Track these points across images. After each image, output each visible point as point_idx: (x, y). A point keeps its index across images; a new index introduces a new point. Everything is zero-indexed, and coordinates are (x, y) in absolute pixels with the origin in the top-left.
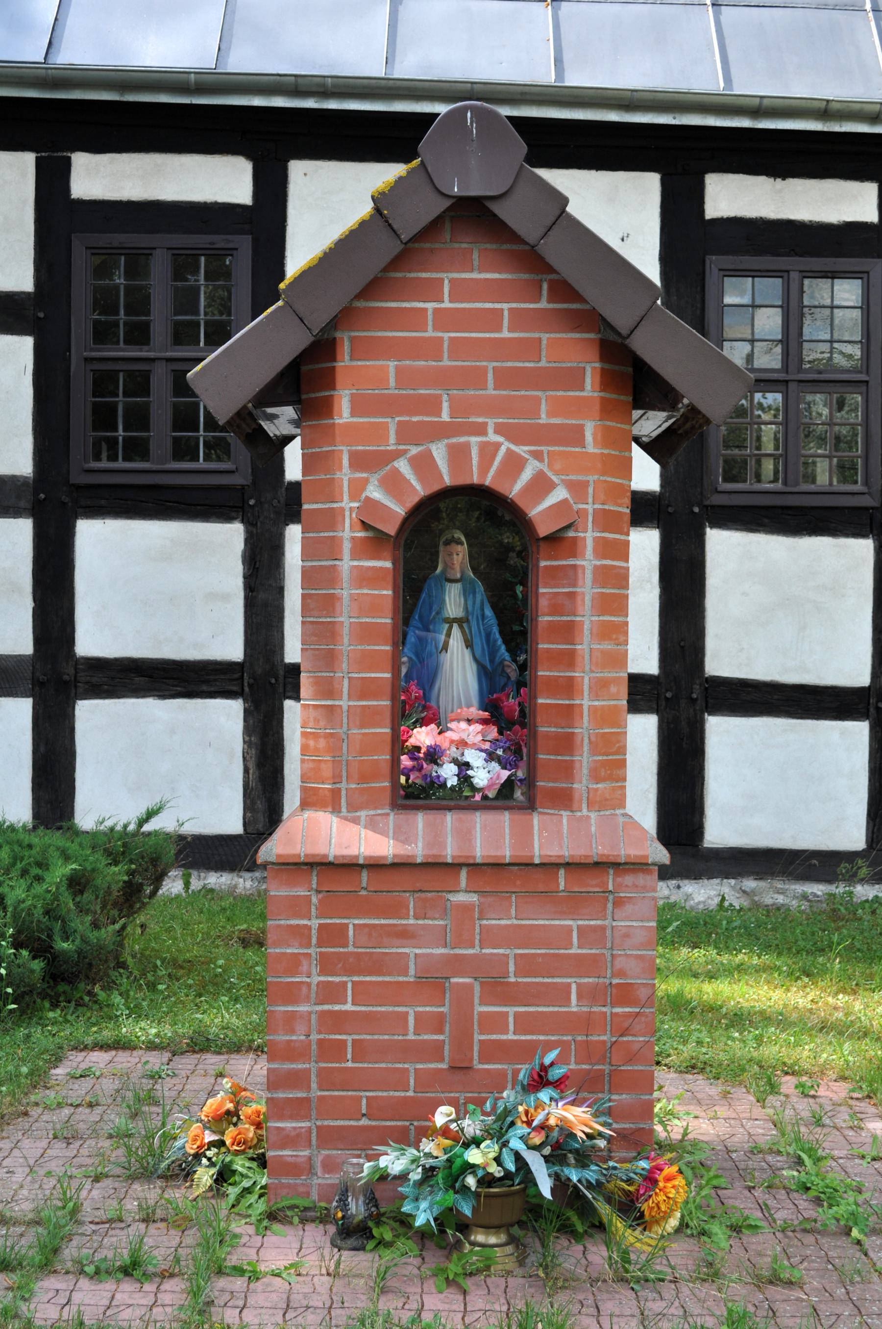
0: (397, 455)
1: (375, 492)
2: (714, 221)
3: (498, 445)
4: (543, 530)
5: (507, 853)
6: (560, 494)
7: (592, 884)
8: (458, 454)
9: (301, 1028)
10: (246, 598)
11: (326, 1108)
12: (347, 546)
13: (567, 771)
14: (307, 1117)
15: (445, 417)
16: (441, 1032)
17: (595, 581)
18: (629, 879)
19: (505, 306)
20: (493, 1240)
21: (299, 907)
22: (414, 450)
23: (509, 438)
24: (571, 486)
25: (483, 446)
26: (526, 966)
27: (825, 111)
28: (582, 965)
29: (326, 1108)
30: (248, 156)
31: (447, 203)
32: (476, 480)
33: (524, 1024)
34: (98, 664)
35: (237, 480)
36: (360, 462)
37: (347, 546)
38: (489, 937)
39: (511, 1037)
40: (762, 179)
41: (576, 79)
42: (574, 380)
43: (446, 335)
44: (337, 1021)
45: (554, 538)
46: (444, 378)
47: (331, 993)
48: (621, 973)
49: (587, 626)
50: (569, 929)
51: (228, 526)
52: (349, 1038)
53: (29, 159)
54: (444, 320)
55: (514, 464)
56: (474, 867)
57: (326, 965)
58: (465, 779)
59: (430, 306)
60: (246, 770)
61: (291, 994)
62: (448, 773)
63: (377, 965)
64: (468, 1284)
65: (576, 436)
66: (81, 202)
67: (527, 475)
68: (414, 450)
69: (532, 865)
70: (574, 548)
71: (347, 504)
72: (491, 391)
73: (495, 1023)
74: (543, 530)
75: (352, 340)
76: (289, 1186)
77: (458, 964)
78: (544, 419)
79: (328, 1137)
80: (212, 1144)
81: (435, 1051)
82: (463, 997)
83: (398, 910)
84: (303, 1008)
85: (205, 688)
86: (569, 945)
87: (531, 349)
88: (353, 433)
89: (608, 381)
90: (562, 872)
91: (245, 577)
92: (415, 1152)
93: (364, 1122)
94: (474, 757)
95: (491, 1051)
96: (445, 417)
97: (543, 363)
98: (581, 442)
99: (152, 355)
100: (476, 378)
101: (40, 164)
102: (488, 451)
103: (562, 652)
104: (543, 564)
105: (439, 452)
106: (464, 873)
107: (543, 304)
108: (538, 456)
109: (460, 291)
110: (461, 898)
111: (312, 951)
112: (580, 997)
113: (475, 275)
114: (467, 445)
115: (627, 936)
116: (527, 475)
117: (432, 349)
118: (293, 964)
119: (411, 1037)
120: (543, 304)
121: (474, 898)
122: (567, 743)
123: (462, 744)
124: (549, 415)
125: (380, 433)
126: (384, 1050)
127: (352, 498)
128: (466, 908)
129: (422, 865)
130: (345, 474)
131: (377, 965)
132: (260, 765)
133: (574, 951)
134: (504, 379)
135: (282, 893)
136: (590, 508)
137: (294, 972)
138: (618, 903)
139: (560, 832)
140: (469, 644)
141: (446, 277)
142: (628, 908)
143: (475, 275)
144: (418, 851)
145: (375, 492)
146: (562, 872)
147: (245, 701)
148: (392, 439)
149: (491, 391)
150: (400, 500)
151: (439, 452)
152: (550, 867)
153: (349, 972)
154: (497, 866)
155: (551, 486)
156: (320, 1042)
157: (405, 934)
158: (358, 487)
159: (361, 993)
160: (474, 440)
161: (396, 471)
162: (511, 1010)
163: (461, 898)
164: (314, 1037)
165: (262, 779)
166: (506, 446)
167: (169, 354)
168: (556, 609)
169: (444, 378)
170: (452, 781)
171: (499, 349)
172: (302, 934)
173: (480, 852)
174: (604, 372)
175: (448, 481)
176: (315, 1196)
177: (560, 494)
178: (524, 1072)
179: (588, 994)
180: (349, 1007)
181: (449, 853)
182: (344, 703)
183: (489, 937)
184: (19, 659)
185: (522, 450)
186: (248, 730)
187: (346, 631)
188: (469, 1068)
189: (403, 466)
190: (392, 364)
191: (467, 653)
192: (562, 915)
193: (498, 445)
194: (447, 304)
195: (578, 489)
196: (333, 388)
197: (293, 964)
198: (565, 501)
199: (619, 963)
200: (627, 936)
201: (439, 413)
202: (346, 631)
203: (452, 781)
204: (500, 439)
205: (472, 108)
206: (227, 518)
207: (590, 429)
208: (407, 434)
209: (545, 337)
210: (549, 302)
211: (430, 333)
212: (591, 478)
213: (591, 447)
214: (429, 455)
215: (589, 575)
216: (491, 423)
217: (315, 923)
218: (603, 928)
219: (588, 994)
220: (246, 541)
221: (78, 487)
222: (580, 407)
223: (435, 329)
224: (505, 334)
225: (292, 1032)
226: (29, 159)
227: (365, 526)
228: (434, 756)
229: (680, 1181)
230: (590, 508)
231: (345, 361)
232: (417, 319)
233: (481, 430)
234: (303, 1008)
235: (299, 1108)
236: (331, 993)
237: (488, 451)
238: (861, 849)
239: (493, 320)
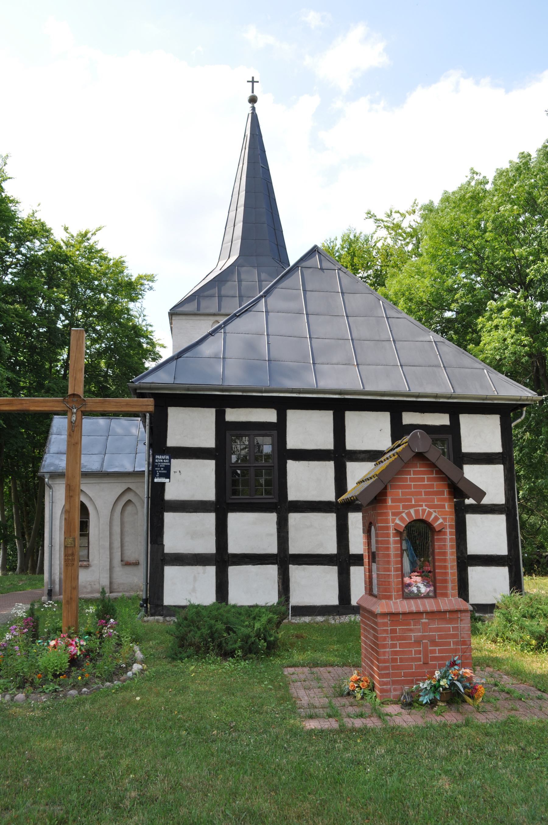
0: (403, 512)
1: (397, 521)
2: (405, 425)
3: (426, 509)
4: (437, 530)
5: (435, 609)
6: (441, 521)
7: (455, 616)
8: (417, 512)
9: (387, 655)
10: (278, 535)
11: (394, 675)
12: (391, 535)
13: (446, 588)
14: (389, 677)
15: (413, 503)
16: (420, 654)
17: (450, 542)
18: (463, 614)
19: (426, 476)
20: (443, 705)
21: (385, 624)
22: (406, 511)
23: (428, 507)
24: (443, 519)
25: (422, 510)
26: (440, 637)
27: (436, 396)
28: (454, 636)
29: (394, 675)
30: (275, 409)
31: (414, 454)
32: (421, 518)
33: (440, 651)
34: (235, 556)
35: (275, 501)
36: (394, 514)
37: (391, 535)
38: (431, 630)
39: (437, 655)
40: (418, 413)
41: (368, 388)
42: (442, 493)
43: (412, 483)
44: (395, 653)
45: (440, 531)
46: (412, 494)
47: (394, 646)
48: (463, 638)
49: (449, 552)
50: (450, 627)
51: (272, 514)
52: (398, 657)
53: (213, 411)
54: (412, 480)
55: (430, 514)
56: (427, 613)
57: (392, 639)
58: (419, 591)
59: (408, 476)
60: (279, 586)
61: (384, 646)
62: (415, 589)
63: (404, 638)
64: (442, 714)
65: (443, 507)
66: (228, 422)
67: (433, 516)
68: (406, 511)
69: (441, 612)
70: (445, 534)
71: (391, 524)
72: (423, 496)
73: (433, 651)
74: (437, 530)
75: (391, 485)
76: (385, 695)
77: (424, 637)
78: (436, 503)
79: (394, 682)
80: (357, 687)
81: (419, 659)
82: (425, 647)
83: (409, 624)
84: (387, 650)
85: (266, 562)
86: (450, 631)
87: (432, 486)
88: (392, 507)
89: (450, 493)
90: (448, 613)
91: (277, 529)
92: (333, 702)
93: (403, 678)
94: (420, 585)
95: (434, 659)
96: (413, 503)
97: (435, 490)
98: (445, 508)
99: (249, 465)
100: (420, 493)
101: (216, 411)
102: (424, 511)
103: (442, 559)
104: (435, 537)
105: (412, 511)
106: (424, 615)
107: (434, 476)
108: (435, 512)
109: (415, 473)
110: (424, 621)
111: (389, 635)
112: (453, 644)
113: (418, 469)
114: (419, 509)
115: (464, 628)
116: (433, 516)
117: (409, 487)
118: (385, 639)
119: (413, 656)
120: (434, 476)
121: (427, 621)
122: (446, 581)
123: (416, 582)
124: (437, 501)
125: (398, 507)
126: (407, 660)
127: (392, 523)
128: (425, 623)
129: (416, 613)
130: (391, 517)
131: (404, 638)
132: (283, 584)
133: (451, 632)
134: (427, 493)
135: (381, 621)
136: (448, 524)
137: (385, 641)
138: (461, 620)
139: (446, 603)
140: (408, 556)
141: (412, 470)
142: (464, 622)
143: (418, 469)
144: (414, 609)
145: (397, 521)
146: (448, 613)
147: (278, 565)
148: (401, 508)
149: (423, 496)
150: (403, 523)
151: (412, 511)
152: (445, 612)
153: (398, 640)
154: (432, 613)
155: (438, 519)
156: (391, 658)
157: (411, 630)
158: (393, 520)
159: (401, 645)
160: (420, 508)
161: (402, 516)
162: (437, 648)
163: (424, 621)
164: (390, 657)
165: (283, 589)
166: (428, 509)
167: (254, 465)
168: (440, 548)
169: (412, 494)
170: (416, 592)
171: (425, 486)
172: (386, 631)
173: (429, 609)
174: (449, 491)
175: (415, 518)
176: (392, 698)
177: (441, 521)
178: (447, 663)
179: (455, 643)
180: (398, 649)
181: (422, 609)
182: (393, 573)
183: (431, 630)
184: (212, 554)
185: (431, 510)
186: (279, 574)
187: (392, 555)
188: (428, 663)
189: (404, 515)
190: (400, 491)
191: (408, 558)
192: (448, 624)
193: (426, 509)
194: (412, 476)
195: (444, 519)
196: (386, 496)
197: (385, 639)
198: (442, 523)
199: (462, 635)
200: (464, 628)
201: (412, 502)
202: (392, 555)
203: (416, 592)
204: (426, 508)
205: (419, 432)
206: (272, 512)
207: (446, 505)
208: (405, 507)
209: (435, 483)
210: (436, 474)
211: (409, 483)
212: (448, 517)
213: (447, 509)
214: (410, 512)
215: (448, 540)
216: (424, 504)
217: (389, 628)
218: (458, 627)
219: (455, 643)
220: (277, 518)
221: (228, 504)
222: (444, 500)
223: (410, 482)
224: (426, 483)
225: (385, 656)
226: (213, 411)
227: (395, 529)
228: (409, 585)
229: (483, 688)
230: (448, 524)
231: (389, 490)
232: (405, 480)
233: (422, 506)
234: (387, 650)
235: (387, 675)
236: (394, 646)
237: (424, 511)
238: (208, 604)
239: (423, 479)
